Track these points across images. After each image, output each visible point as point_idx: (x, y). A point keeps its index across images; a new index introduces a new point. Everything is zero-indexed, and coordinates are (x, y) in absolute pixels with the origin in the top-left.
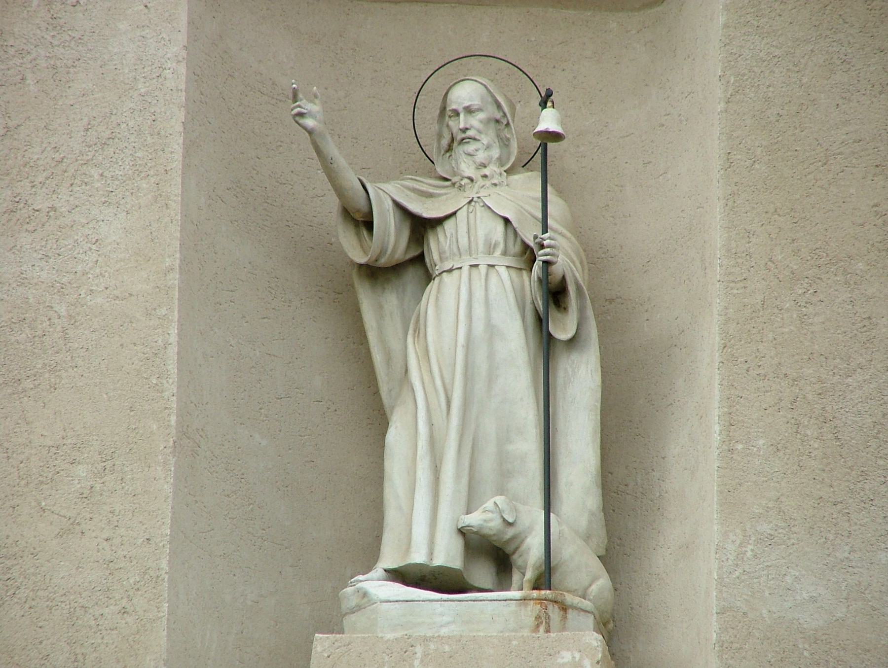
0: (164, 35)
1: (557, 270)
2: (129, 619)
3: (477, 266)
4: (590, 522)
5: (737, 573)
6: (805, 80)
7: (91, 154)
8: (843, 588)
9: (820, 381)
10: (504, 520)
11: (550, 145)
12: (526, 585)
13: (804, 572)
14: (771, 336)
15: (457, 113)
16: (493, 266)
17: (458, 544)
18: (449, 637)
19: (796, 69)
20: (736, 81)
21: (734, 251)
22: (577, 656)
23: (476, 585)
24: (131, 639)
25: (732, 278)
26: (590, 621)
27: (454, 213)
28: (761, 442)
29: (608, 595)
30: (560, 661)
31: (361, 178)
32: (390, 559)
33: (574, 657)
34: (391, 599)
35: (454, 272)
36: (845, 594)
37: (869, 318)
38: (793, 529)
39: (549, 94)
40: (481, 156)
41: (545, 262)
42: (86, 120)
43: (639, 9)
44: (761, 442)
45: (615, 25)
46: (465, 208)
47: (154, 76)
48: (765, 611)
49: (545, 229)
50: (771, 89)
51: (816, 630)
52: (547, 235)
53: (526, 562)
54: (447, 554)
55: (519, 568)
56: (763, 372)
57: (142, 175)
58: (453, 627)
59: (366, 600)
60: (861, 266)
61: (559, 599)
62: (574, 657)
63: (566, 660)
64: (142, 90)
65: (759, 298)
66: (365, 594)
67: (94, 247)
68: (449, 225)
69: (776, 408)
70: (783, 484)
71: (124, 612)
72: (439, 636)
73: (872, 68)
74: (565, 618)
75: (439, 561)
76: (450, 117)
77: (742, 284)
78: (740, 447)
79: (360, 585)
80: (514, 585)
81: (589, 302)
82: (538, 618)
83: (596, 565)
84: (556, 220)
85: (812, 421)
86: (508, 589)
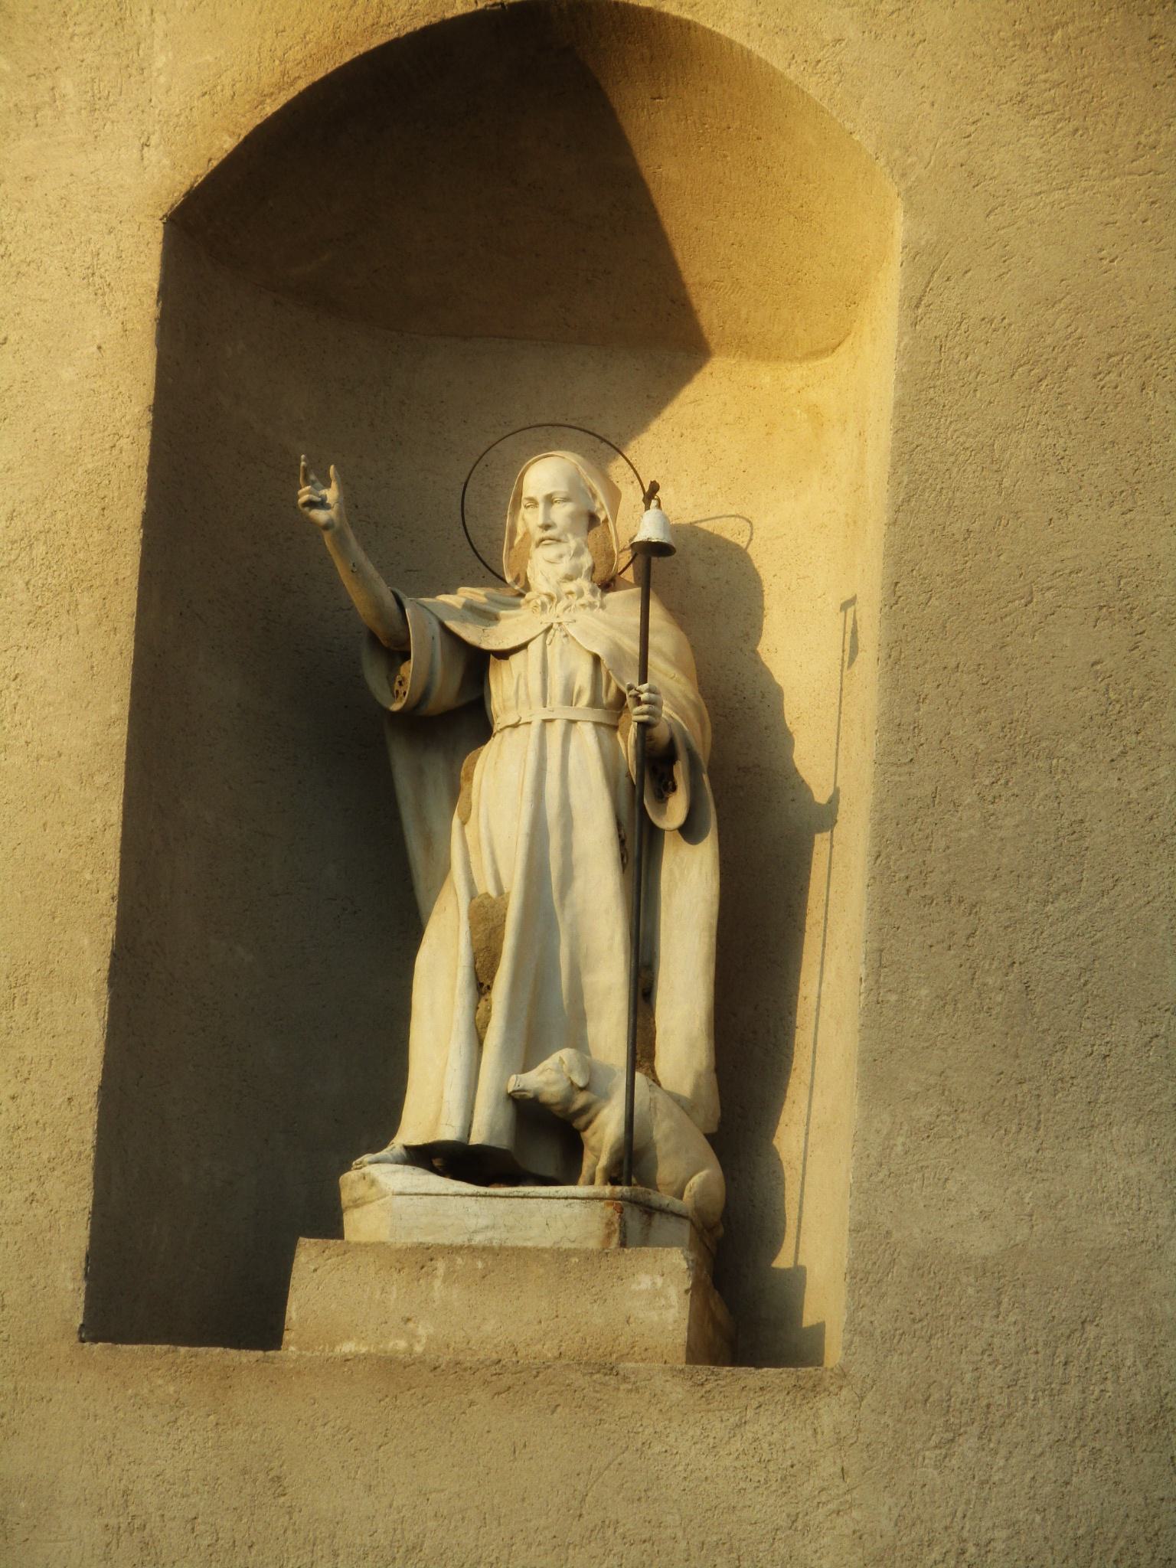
0: (122, 389)
1: (661, 733)
2: (41, 1211)
3: (551, 721)
4: (697, 1087)
5: (881, 1176)
6: (1007, 482)
7: (14, 553)
8: (1027, 1200)
9: (1008, 908)
10: (572, 1083)
11: (654, 559)
12: (598, 1180)
13: (973, 1177)
14: (943, 844)
15: (533, 502)
16: (574, 722)
17: (506, 1115)
18: (484, 1249)
19: (995, 467)
20: (910, 482)
21: (897, 721)
22: (659, 1281)
23: (534, 1171)
24: (39, 1239)
25: (892, 759)
26: (685, 1231)
27: (524, 646)
28: (924, 992)
29: (718, 1191)
30: (634, 1287)
31: (397, 591)
32: (413, 1130)
33: (654, 1283)
34: (408, 1191)
35: (521, 728)
36: (1028, 1209)
37: (1082, 821)
38: (962, 1116)
39: (654, 488)
40: (1154, 127)
41: (640, 723)
42: (10, 504)
43: (801, 360)
44: (924, 992)
45: (768, 379)
46: (538, 642)
47: (107, 446)
48: (916, 1231)
49: (643, 679)
50: (958, 494)
51: (985, 1258)
52: (645, 686)
53: (601, 1141)
54: (486, 1127)
55: (593, 1149)
56: (930, 893)
57: (85, 585)
58: (490, 1234)
59: (374, 1190)
60: (1073, 747)
61: (641, 1198)
62: (654, 1283)
63: (643, 1287)
64: (90, 466)
65: (929, 788)
66: (373, 1183)
67: (13, 685)
68: (515, 659)
69: (945, 945)
70: (950, 1052)
71: (32, 1199)
72: (469, 1247)
73: (1101, 469)
74: (649, 1225)
75: (478, 1137)
76: (526, 507)
77: (906, 769)
78: (893, 998)
79: (368, 1169)
80: (581, 1180)
81: (705, 777)
82: (609, 1224)
83: (701, 1148)
84: (667, 660)
85: (996, 964)
86: (573, 1181)
